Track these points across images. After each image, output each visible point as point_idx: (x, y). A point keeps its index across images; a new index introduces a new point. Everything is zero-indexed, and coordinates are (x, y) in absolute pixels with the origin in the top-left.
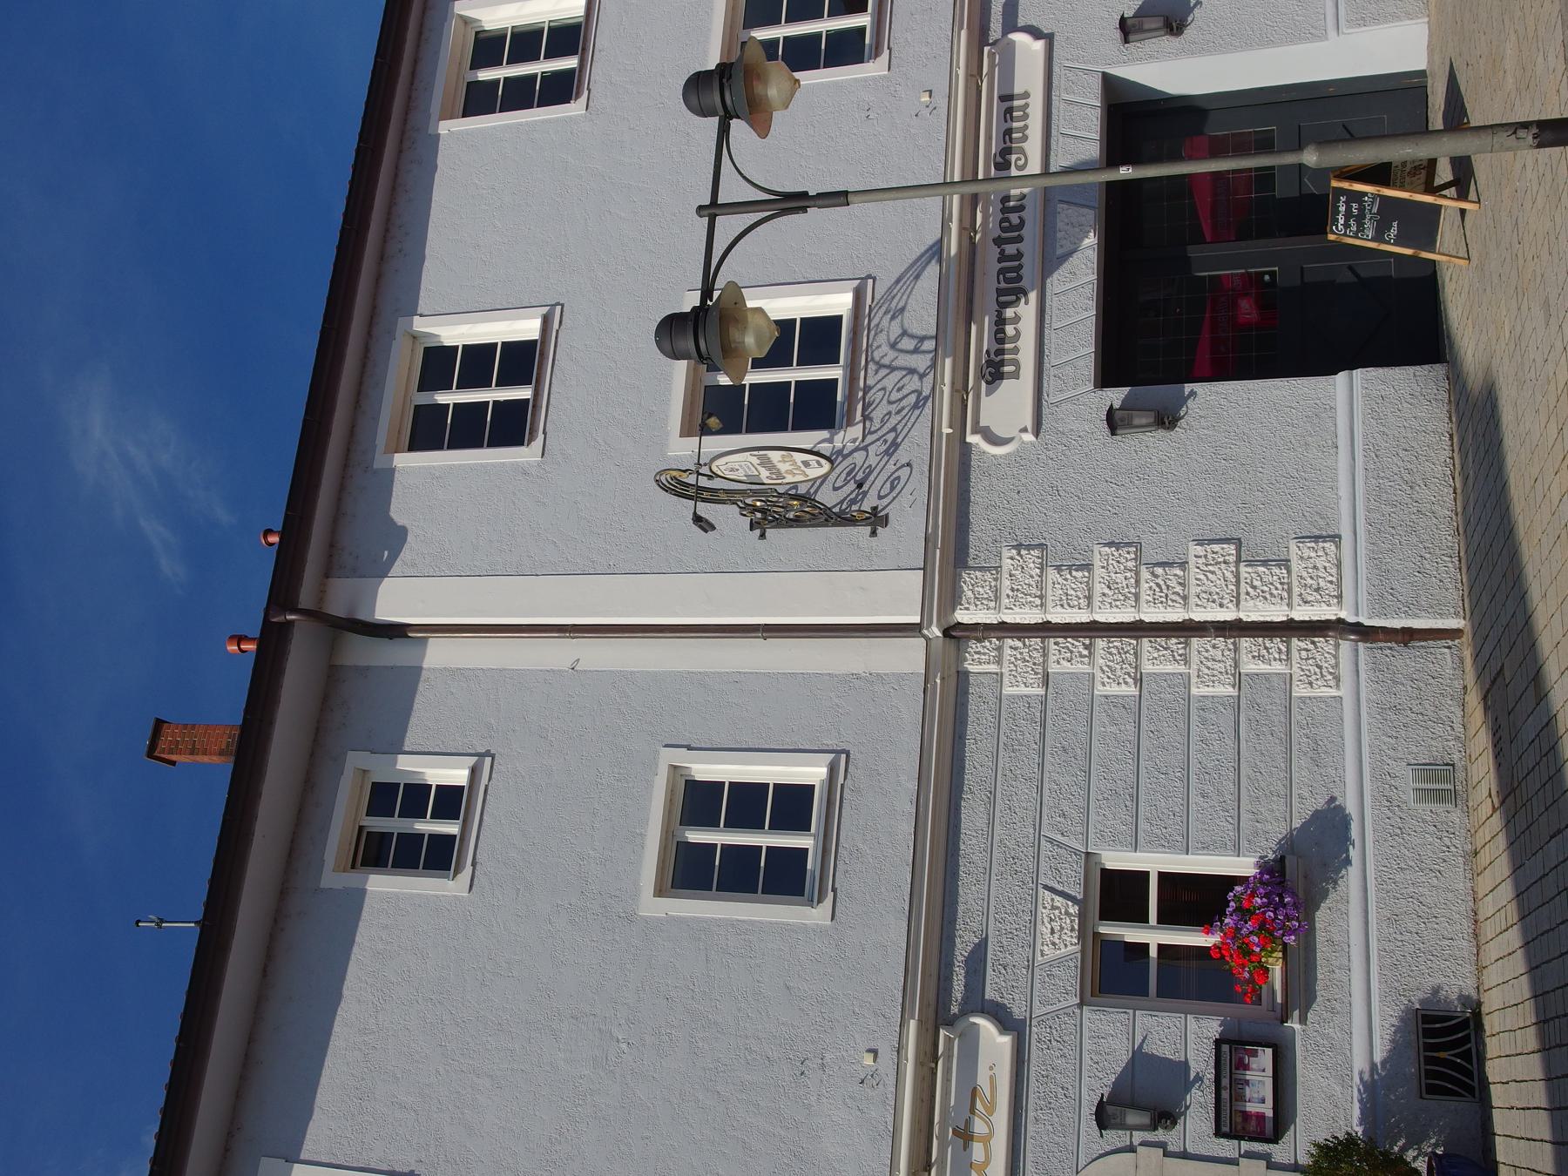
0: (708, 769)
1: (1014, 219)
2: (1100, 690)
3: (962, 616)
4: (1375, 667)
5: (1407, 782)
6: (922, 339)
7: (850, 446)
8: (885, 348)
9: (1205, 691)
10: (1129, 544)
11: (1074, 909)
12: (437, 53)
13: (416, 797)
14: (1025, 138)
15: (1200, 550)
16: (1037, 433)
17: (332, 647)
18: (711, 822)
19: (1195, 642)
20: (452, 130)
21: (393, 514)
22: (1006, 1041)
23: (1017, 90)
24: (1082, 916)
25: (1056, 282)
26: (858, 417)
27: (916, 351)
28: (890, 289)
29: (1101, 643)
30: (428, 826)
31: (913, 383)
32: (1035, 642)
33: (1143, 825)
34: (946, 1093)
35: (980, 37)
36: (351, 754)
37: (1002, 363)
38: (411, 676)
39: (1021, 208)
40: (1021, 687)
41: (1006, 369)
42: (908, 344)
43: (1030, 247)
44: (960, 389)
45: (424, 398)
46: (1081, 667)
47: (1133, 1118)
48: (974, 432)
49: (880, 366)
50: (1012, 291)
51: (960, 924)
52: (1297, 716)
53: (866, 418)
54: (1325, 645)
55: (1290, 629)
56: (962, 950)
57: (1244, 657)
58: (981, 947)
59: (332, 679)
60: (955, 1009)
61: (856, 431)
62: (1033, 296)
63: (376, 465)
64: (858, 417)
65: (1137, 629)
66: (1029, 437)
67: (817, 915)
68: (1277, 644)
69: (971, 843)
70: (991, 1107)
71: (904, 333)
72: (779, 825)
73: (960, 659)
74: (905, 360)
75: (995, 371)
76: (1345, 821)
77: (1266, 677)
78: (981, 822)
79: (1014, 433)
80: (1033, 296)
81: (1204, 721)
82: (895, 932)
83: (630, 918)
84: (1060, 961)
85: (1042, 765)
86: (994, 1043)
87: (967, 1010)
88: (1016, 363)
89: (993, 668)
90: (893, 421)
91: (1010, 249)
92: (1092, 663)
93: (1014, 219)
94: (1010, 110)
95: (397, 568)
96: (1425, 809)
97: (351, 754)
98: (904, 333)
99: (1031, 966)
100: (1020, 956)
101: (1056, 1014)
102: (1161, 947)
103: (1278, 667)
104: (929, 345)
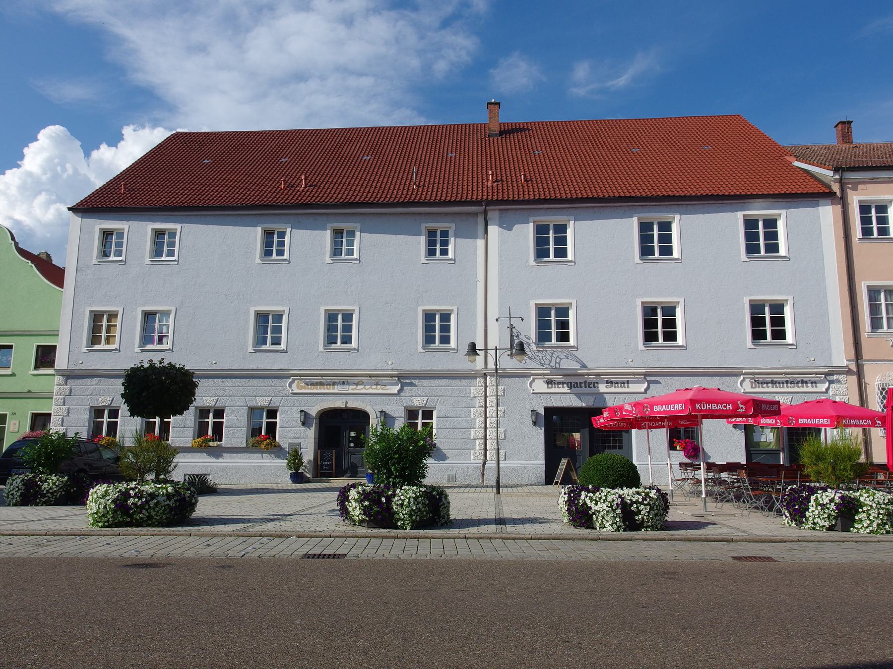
0: (453, 318)
1: (592, 385)
2: (472, 409)
3: (488, 377)
4: (477, 467)
5: (452, 473)
6: (559, 364)
7: (531, 348)
8: (557, 355)
9: (472, 432)
10: (504, 415)
11: (424, 405)
12: (662, 212)
13: (445, 243)
14: (615, 387)
15: (502, 431)
16: (532, 393)
17: (481, 213)
18: (343, 320)
19: (483, 430)
20: (633, 223)
21: (516, 226)
22: (396, 392)
23: (630, 385)
24: (422, 406)
25: (573, 396)
26: (538, 349)
27: (556, 362)
28: (573, 355)
29: (483, 409)
30: (438, 247)
31: (547, 362)
32: (483, 394)
33: (442, 419)
34: (767, 378)
35: (646, 375)
36: (454, 224)
37: (552, 384)
38: (475, 237)
39: (595, 387)
40: (473, 391)
41: (550, 386)
42: (558, 360)
43: (584, 390)
44: (544, 375)
45: (551, 227)
46: (478, 405)
47: (382, 418)
48: (744, 378)
49: (552, 354)
50: (571, 386)
51: (419, 380)
52: (467, 451)
53: (538, 351)
54: (482, 458)
55: (485, 450)
56: (414, 381)
57: (480, 440)
58: (415, 385)
59: (475, 214)
60: (402, 380)
61: (535, 349)
62: (569, 391)
63: (530, 218)
64: (538, 349)
65: (486, 417)
66: (532, 391)
67: (420, 349)
68: (483, 447)
69: (437, 382)
70: (382, 389)
71: (561, 359)
72: (441, 337)
73: (479, 377)
74: (554, 359)
75: (549, 383)
76: (444, 461)
77: (476, 445)
78: (442, 384)
79: (533, 388)
80: (569, 391)
81: (465, 432)
82: (417, 367)
83: (417, 305)
84: (256, 402)
85: (455, 397)
86: (395, 389)
87: (401, 382)
88: (552, 387)
89: (477, 385)
90: (537, 358)
91: (583, 385)
92: (479, 407)
93: (592, 385)
94: (624, 383)
95: (501, 230)
96: (446, 476)
97: (454, 224)
98: (561, 359)
99: (411, 396)
100: (414, 394)
101: (402, 402)
102: (208, 422)
103: (478, 447)
104: (557, 366)
